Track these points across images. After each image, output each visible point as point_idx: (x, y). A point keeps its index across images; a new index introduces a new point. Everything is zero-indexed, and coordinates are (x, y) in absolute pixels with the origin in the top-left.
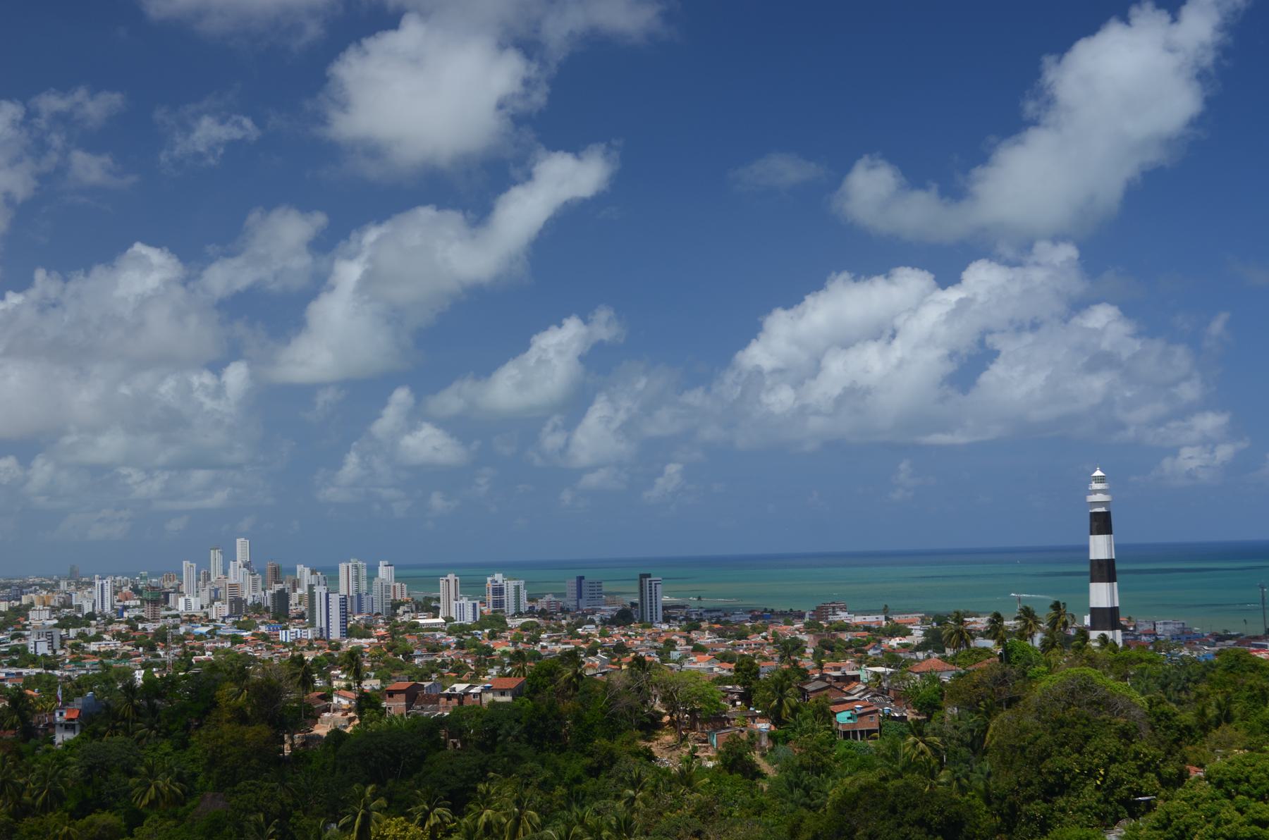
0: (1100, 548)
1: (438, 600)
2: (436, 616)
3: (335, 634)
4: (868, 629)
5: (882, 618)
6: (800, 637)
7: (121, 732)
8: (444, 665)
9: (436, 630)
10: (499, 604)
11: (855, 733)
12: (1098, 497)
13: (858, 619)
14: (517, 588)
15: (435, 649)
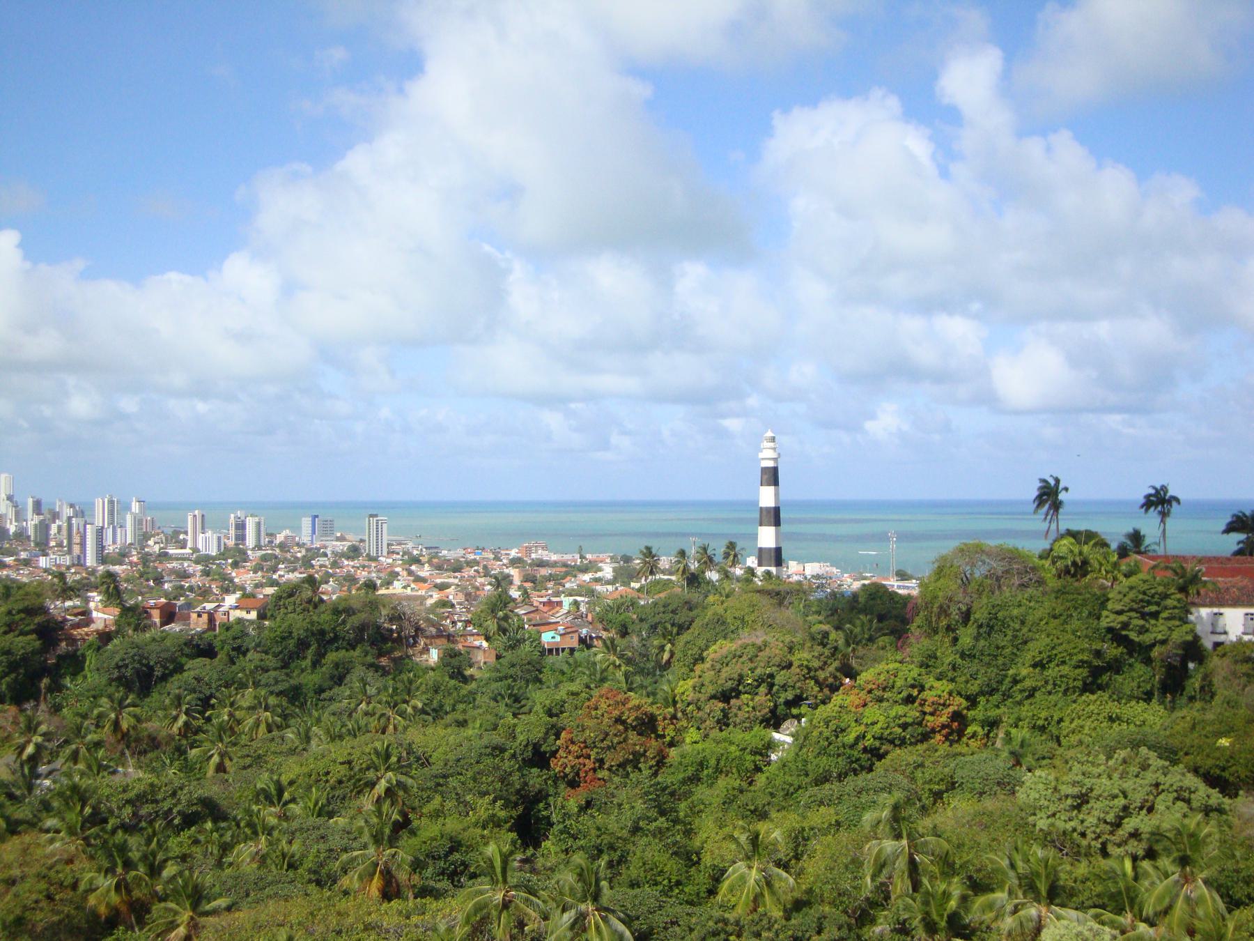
0: (767, 497)
1: (186, 533)
2: (184, 547)
3: (90, 561)
4: (565, 565)
5: (577, 556)
6: (507, 571)
7: (732, 920)
8: (191, 589)
9: (184, 559)
10: (241, 538)
11: (557, 650)
12: (766, 457)
13: (554, 557)
14: (258, 524)
15: (184, 575)
